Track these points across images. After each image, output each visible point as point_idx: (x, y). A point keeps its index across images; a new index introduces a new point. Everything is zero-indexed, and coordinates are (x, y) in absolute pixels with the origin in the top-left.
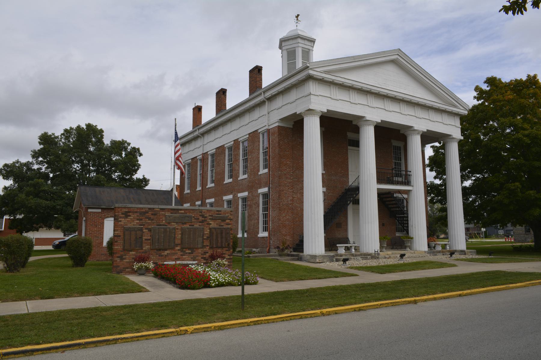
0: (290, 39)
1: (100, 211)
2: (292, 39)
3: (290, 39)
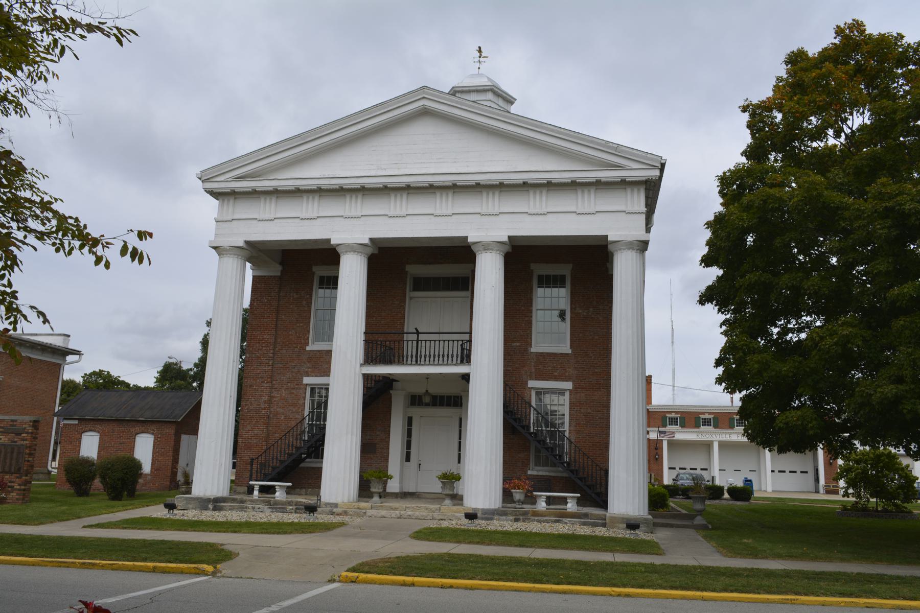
0: (473, 91)
1: (76, 422)
2: (478, 91)
3: (473, 91)
